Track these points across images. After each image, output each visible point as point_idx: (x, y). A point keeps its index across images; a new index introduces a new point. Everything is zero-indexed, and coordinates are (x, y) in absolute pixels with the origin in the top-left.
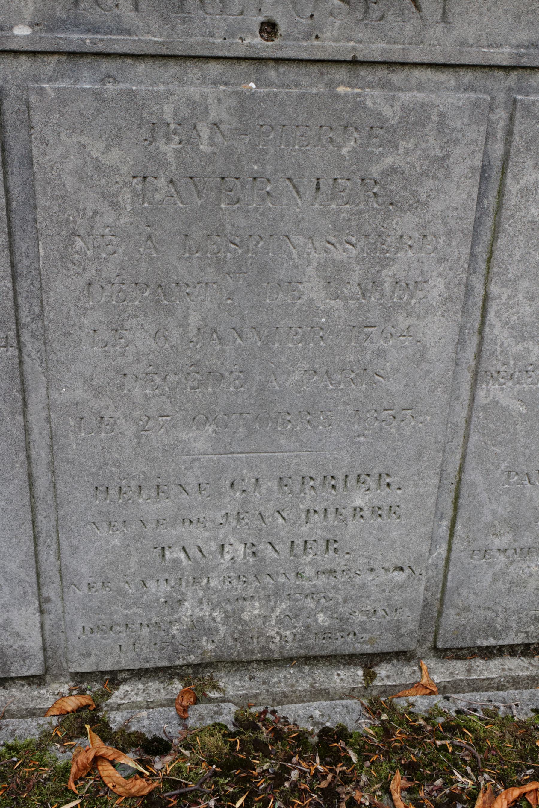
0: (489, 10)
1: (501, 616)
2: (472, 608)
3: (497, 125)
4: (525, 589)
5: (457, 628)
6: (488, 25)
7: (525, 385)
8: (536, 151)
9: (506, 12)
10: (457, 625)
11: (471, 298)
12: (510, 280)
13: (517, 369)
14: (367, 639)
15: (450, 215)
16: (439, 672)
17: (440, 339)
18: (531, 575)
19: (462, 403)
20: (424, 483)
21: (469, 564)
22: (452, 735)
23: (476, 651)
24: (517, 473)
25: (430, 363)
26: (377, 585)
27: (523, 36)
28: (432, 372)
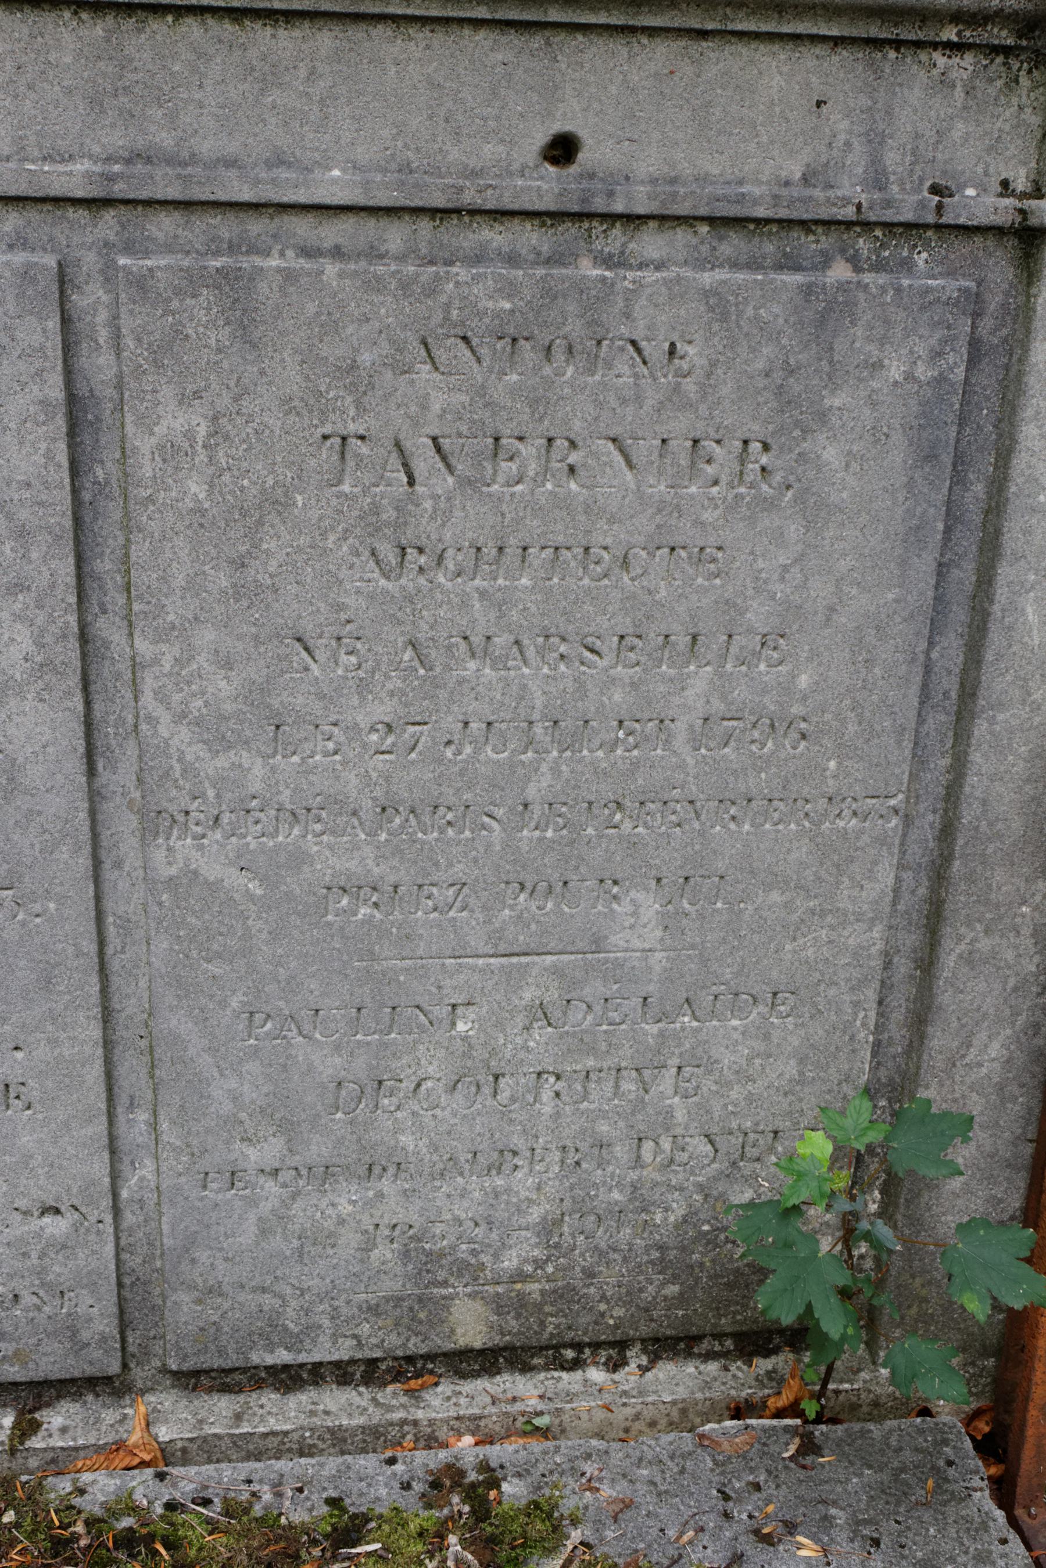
0: (30, 87)
1: (294, 1303)
2: (225, 1288)
3: (94, 316)
4: (335, 1250)
5: (202, 1329)
6: (36, 117)
7: (249, 838)
8: (176, 368)
9: (69, 92)
10: (201, 1324)
11: (107, 663)
12: (173, 628)
13: (224, 807)
14: (10, 1353)
15: (16, 497)
16: (176, 1418)
17: (44, 747)
18: (341, 1222)
19: (129, 874)
20: (69, 1038)
21: (202, 1199)
22: (129, 1556)
23: (263, 1375)
24: (269, 1016)
25: (32, 795)
26: (8, 1244)
27: (117, 139)
28: (40, 813)
